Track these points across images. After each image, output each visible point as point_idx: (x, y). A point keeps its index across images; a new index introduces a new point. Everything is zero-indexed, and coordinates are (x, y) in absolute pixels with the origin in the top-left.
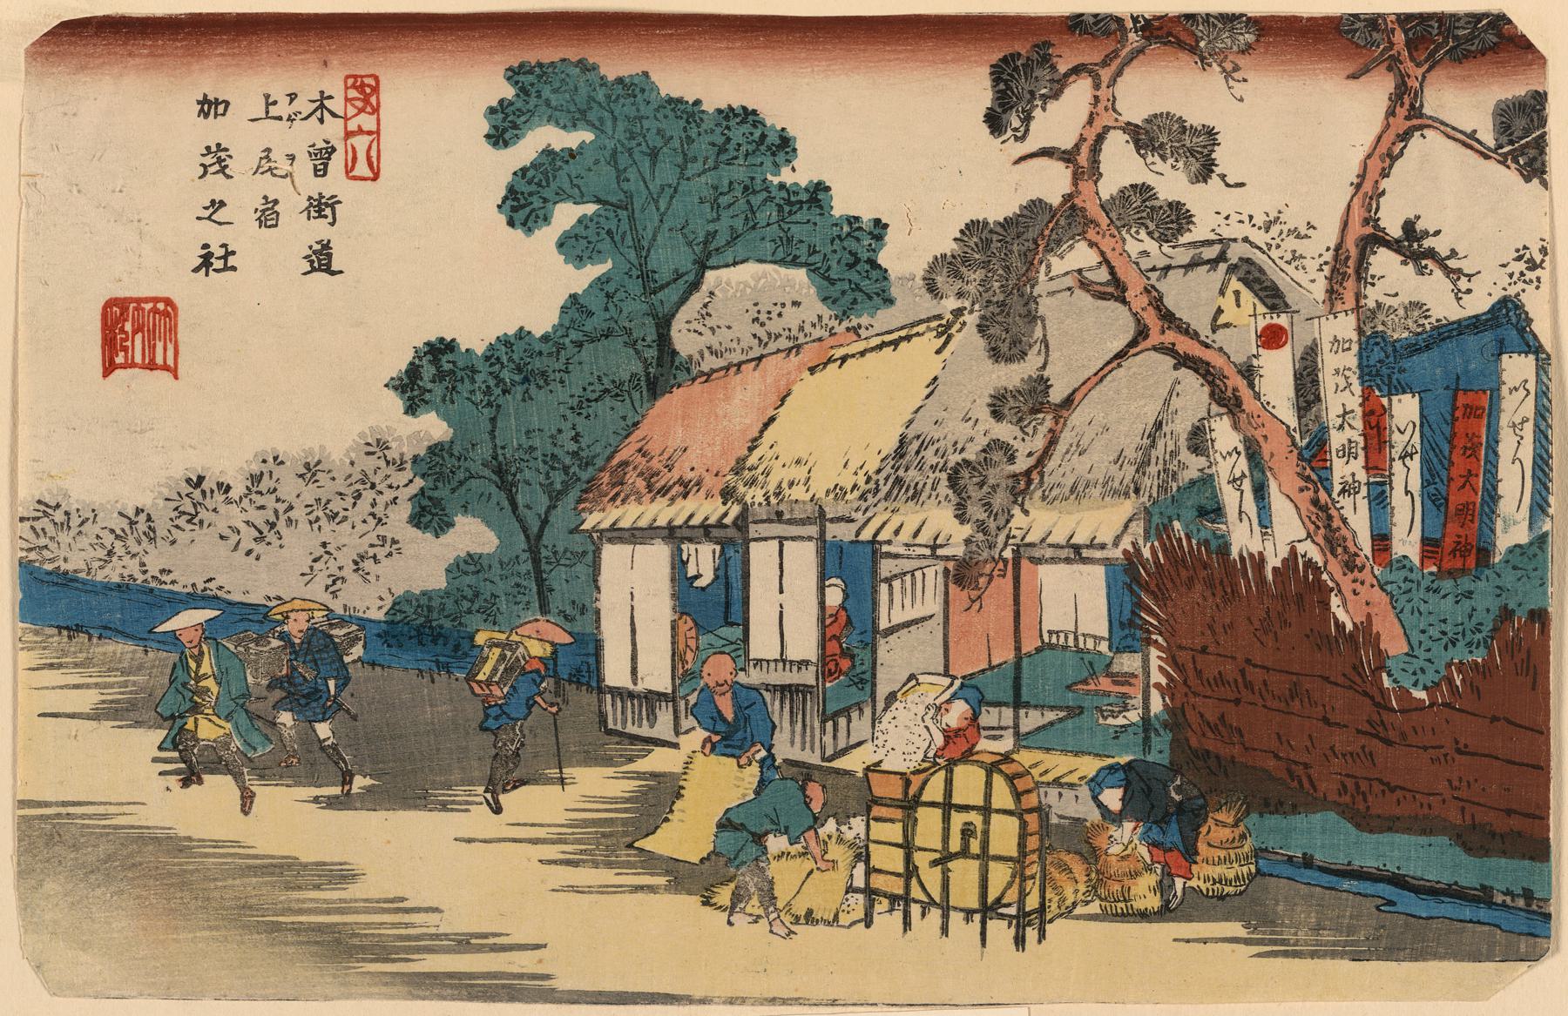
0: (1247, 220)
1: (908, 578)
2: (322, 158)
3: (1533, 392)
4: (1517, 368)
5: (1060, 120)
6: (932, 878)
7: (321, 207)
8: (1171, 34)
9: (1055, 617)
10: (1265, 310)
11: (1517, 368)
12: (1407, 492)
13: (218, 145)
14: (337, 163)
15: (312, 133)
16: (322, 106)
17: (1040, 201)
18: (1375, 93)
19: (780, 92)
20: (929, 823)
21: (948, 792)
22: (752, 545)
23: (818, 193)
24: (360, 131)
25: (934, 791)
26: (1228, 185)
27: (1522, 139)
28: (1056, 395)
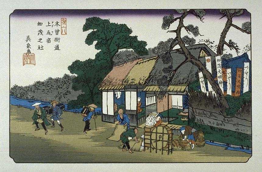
0: (204, 41)
1: (151, 97)
2: (57, 32)
3: (249, 68)
4: (247, 64)
5: (174, 26)
6: (154, 144)
7: (57, 39)
8: (192, 12)
9: (174, 103)
10: (207, 55)
11: (247, 64)
12: (229, 84)
13: (41, 30)
14: (60, 33)
15: (56, 28)
16: (57, 24)
17: (38, 82)
18: (225, 20)
19: (130, 22)
20: (154, 136)
21: (157, 131)
22: (130, 92)
23: (136, 37)
24: (64, 27)
25: (155, 131)
26: (201, 36)
27: (247, 29)
28: (174, 68)
